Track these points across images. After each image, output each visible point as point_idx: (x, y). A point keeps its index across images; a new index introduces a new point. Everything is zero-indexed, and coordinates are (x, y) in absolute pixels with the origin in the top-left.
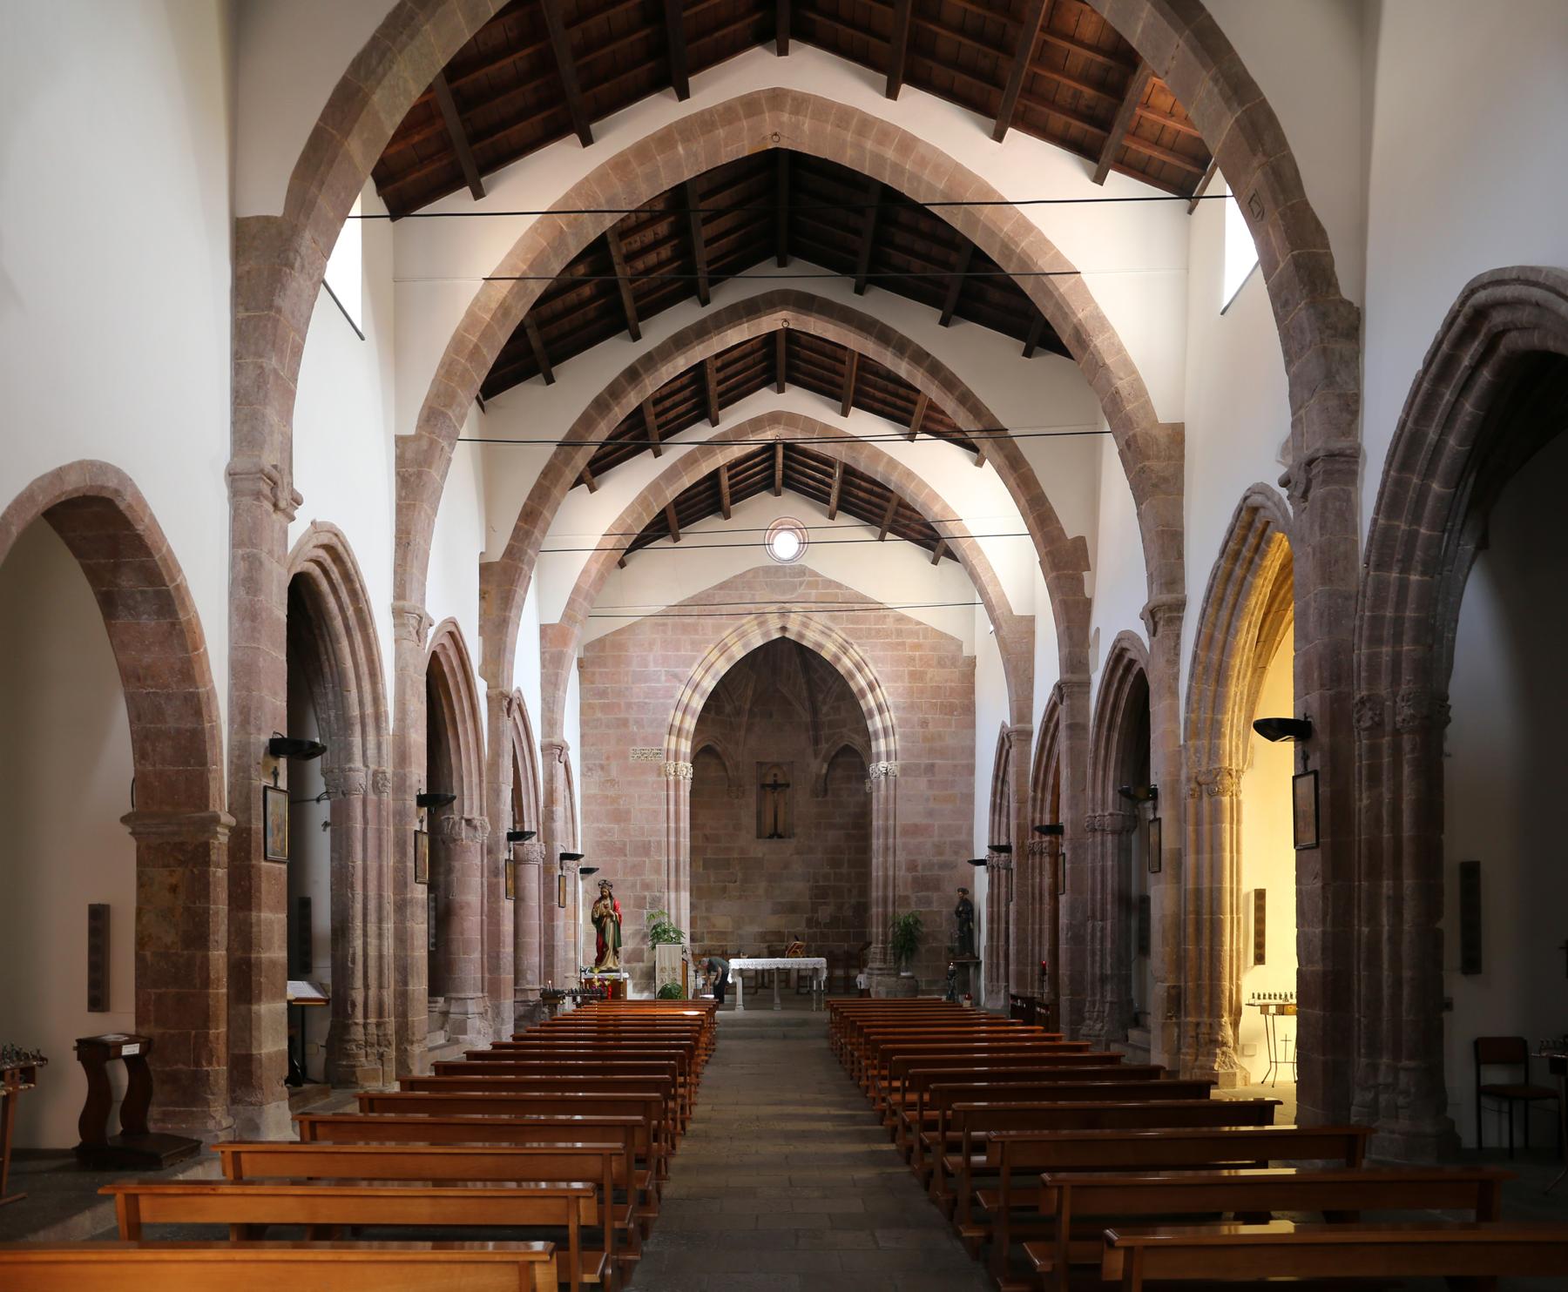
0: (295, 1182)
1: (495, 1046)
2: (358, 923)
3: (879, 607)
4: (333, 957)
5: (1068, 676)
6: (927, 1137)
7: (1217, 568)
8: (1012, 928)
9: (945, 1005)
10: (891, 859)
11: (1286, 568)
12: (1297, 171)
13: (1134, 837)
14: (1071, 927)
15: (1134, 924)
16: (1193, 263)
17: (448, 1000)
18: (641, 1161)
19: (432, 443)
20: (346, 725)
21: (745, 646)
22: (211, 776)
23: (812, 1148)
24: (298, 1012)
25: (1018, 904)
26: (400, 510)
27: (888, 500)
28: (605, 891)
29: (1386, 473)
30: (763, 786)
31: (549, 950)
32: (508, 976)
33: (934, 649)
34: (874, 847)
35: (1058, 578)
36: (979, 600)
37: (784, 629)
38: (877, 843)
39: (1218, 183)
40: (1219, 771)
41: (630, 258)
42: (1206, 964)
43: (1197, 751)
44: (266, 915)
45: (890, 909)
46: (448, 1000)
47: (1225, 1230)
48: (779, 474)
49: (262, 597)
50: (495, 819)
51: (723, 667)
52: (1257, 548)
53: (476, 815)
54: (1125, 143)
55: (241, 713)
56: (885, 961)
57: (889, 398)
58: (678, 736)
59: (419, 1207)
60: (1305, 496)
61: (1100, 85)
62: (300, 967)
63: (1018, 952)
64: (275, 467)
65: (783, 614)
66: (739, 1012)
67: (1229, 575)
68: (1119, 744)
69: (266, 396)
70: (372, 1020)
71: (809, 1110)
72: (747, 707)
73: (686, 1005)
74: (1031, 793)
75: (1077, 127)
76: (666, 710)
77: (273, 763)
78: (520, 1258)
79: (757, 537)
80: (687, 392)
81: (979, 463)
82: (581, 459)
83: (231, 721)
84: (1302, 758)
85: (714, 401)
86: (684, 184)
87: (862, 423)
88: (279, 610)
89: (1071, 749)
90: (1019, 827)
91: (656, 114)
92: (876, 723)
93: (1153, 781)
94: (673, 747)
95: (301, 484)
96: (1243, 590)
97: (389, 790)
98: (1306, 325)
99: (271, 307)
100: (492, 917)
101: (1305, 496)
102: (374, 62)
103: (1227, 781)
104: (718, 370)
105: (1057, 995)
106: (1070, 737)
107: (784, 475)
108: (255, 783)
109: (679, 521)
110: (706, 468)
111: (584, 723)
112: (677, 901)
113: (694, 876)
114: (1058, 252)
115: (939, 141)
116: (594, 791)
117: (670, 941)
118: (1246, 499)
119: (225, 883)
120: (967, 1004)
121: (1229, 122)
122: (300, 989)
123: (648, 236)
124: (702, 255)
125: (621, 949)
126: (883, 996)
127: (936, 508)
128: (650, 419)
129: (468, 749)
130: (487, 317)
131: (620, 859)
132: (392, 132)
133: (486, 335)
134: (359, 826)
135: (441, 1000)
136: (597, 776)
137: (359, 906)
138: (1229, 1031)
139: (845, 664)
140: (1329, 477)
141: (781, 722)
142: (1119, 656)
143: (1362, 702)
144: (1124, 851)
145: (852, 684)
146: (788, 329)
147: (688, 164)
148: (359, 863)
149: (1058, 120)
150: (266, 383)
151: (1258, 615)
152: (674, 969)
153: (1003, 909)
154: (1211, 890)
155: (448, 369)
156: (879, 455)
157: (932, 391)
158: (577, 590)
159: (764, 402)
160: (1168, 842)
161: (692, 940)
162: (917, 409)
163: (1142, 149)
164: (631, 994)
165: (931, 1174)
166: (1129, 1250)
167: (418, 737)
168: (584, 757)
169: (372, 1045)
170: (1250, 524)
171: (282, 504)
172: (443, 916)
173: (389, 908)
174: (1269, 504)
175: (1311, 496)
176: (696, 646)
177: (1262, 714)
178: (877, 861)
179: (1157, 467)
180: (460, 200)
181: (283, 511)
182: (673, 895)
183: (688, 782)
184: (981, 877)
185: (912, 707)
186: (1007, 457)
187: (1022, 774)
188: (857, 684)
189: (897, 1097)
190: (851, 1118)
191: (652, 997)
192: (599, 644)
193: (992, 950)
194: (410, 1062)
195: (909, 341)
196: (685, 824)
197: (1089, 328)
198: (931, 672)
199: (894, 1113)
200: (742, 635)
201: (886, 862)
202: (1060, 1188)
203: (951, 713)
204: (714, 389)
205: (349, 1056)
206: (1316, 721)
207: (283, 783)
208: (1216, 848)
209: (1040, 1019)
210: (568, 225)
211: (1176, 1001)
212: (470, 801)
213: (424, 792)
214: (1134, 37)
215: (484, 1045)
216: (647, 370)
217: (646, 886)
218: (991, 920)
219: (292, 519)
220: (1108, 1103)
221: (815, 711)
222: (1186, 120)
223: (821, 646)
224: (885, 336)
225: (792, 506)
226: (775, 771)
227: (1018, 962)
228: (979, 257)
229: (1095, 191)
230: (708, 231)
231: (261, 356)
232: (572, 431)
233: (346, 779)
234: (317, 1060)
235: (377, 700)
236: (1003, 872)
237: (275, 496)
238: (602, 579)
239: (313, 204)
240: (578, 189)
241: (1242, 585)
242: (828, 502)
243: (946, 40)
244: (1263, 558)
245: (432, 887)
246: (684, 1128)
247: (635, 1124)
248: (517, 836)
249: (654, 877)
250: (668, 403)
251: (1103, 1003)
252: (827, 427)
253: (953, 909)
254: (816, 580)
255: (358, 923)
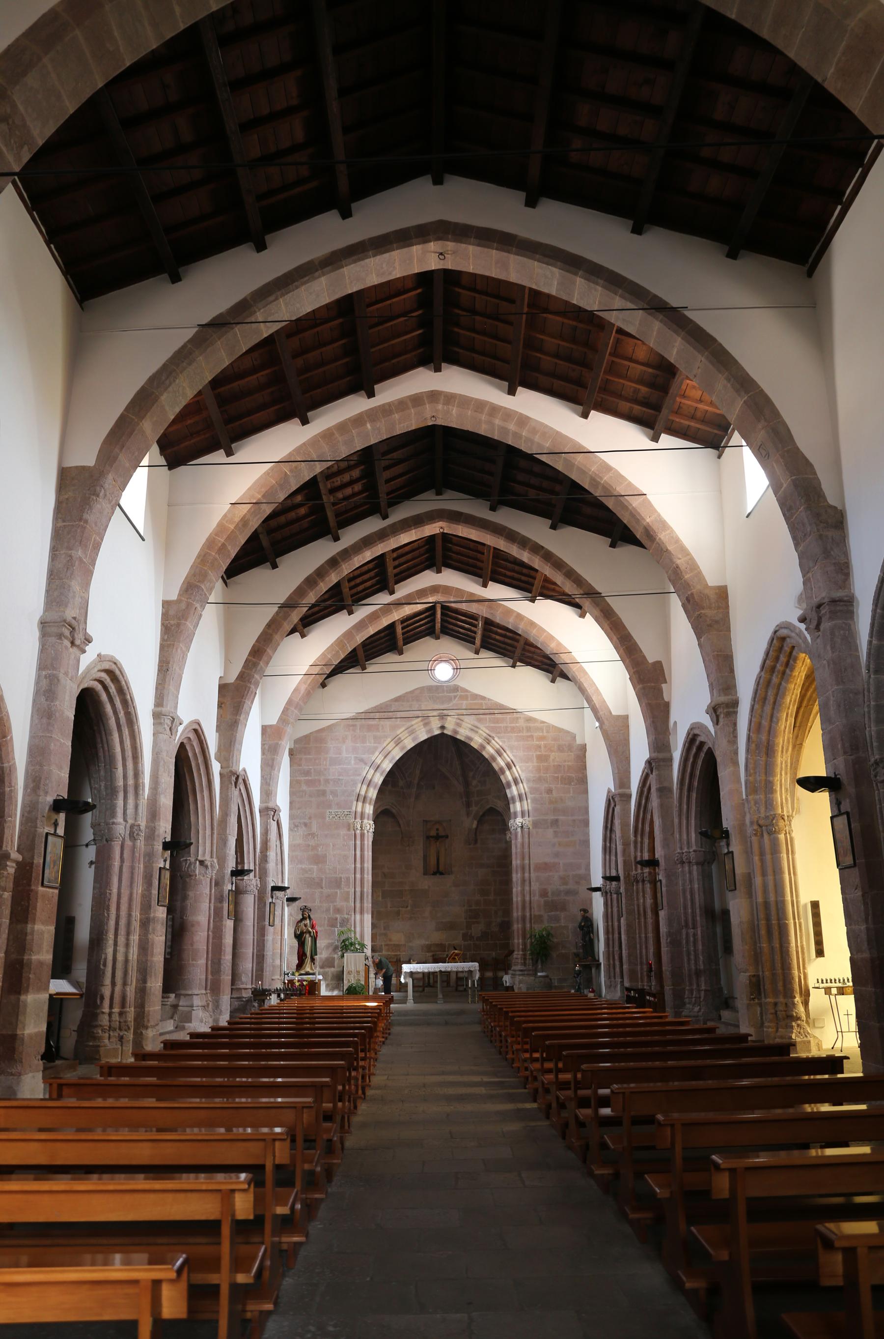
0: (41, 1130)
1: (213, 1028)
2: (111, 935)
3: (514, 711)
4: (89, 962)
5: (655, 755)
6: (562, 1095)
7: (759, 678)
8: (623, 937)
9: (573, 995)
10: (527, 888)
11: (810, 678)
12: (789, 430)
13: (714, 867)
14: (669, 934)
15: (719, 930)
16: (724, 491)
17: (178, 996)
18: (328, 1117)
19: (189, 605)
20: (112, 791)
21: (414, 739)
22: (6, 825)
23: (469, 1107)
24: (57, 1003)
25: (627, 919)
26: (162, 648)
27: (518, 641)
28: (306, 914)
29: (874, 611)
30: (428, 837)
31: (260, 958)
32: (227, 977)
33: (555, 739)
34: (514, 879)
35: (644, 688)
36: (586, 705)
37: (443, 727)
38: (516, 877)
39: (736, 438)
40: (774, 817)
41: (333, 491)
42: (778, 958)
43: (756, 803)
44: (38, 927)
45: (528, 925)
46: (178, 996)
47: (813, 1152)
48: (438, 626)
49: (57, 703)
50: (222, 860)
51: (397, 754)
52: (787, 664)
53: (207, 857)
54: (671, 418)
55: (34, 781)
56: (525, 964)
57: (516, 575)
58: (364, 802)
59: (144, 1154)
60: (818, 628)
61: (652, 385)
62: (62, 967)
63: (629, 955)
64: (74, 618)
65: (442, 717)
66: (410, 1005)
67: (769, 683)
68: (698, 802)
69: (72, 574)
70: (116, 1010)
71: (466, 1079)
72: (416, 782)
73: (368, 999)
74: (632, 838)
75: (637, 409)
76: (355, 784)
77: (55, 816)
78: (223, 1187)
79: (424, 666)
80: (372, 574)
81: (582, 616)
82: (295, 616)
83: (26, 787)
84: (836, 804)
85: (391, 580)
86: (371, 446)
87: (495, 591)
88: (69, 712)
89: (661, 806)
90: (625, 862)
91: (354, 406)
92: (513, 791)
93: (725, 825)
94: (359, 809)
95: (92, 627)
96: (779, 692)
97: (142, 839)
98: (806, 520)
99: (81, 519)
100: (217, 933)
101: (818, 628)
102: (164, 378)
103: (781, 823)
104: (394, 559)
105: (662, 987)
106: (660, 797)
107: (442, 626)
108: (40, 830)
109: (366, 656)
110: (385, 622)
111: (292, 794)
112: (362, 921)
113: (374, 903)
114: (630, 483)
115: (543, 419)
116: (299, 841)
117: (356, 951)
118: (775, 632)
119: (9, 903)
120: (591, 995)
121: (739, 403)
122: (60, 986)
123: (346, 477)
124: (383, 489)
125: (317, 957)
126: (524, 990)
127: (553, 645)
128: (345, 590)
129: (204, 810)
130: (232, 527)
131: (318, 891)
132: (172, 417)
133: (231, 537)
134: (116, 863)
135: (173, 996)
136: (302, 831)
137: (112, 923)
138: (801, 1009)
139: (489, 751)
140: (833, 615)
141: (442, 792)
142: (692, 740)
143: (877, 763)
144: (706, 877)
145: (494, 765)
146: (443, 533)
147: (374, 434)
148: (115, 891)
149: (625, 406)
150: (73, 566)
151: (793, 709)
152: (358, 972)
153: (616, 924)
154: (777, 902)
155: (203, 559)
156: (509, 612)
157: (547, 570)
158: (290, 702)
159: (427, 579)
160: (740, 869)
161: (373, 950)
162: (536, 582)
163: (682, 421)
164: (324, 991)
165: (566, 1125)
166: (732, 1171)
167: (167, 801)
168: (292, 817)
169: (115, 1030)
170: (781, 649)
171: (78, 642)
172: (178, 931)
173: (136, 925)
174: (793, 635)
175: (822, 627)
176: (377, 740)
177: (802, 774)
178: (516, 890)
179: (710, 615)
180: (219, 456)
181: (78, 646)
182: (358, 917)
183: (371, 836)
184: (598, 900)
185: (540, 780)
186: (602, 611)
187: (625, 825)
188: (498, 764)
189: (537, 1065)
190: (501, 1085)
191: (341, 994)
192: (306, 739)
193: (609, 954)
194: (144, 1043)
195: (529, 539)
196: (368, 865)
197: (655, 527)
198: (553, 756)
199: (535, 1078)
200: (412, 732)
201: (523, 890)
202: (672, 1126)
203: (570, 784)
204: (391, 571)
205: (95, 1038)
206: (844, 778)
207: (61, 831)
208: (777, 871)
209: (650, 1004)
210: (291, 471)
211: (757, 987)
212: (204, 847)
213: (168, 839)
214: (672, 356)
215: (205, 1029)
216: (344, 560)
217: (338, 910)
218: (607, 932)
219: (84, 652)
220: (709, 1062)
221: (467, 784)
222: (711, 404)
223: (471, 739)
224: (511, 536)
225: (448, 646)
226: (437, 826)
227: (630, 962)
228: (575, 486)
229: (653, 445)
230: (387, 474)
231: (71, 549)
232: (290, 598)
233: (110, 830)
234: (69, 1041)
235: (137, 775)
236: (615, 896)
237: (73, 637)
238: (308, 694)
239: (115, 458)
240: (298, 450)
241: (778, 688)
242: (474, 643)
243: (547, 362)
244: (792, 670)
245: (170, 910)
246: (364, 1093)
247: (323, 1085)
248: (239, 873)
249: (344, 904)
250: (358, 581)
251: (699, 991)
252: (472, 594)
253: (577, 925)
254: (466, 694)
255: (111, 935)
